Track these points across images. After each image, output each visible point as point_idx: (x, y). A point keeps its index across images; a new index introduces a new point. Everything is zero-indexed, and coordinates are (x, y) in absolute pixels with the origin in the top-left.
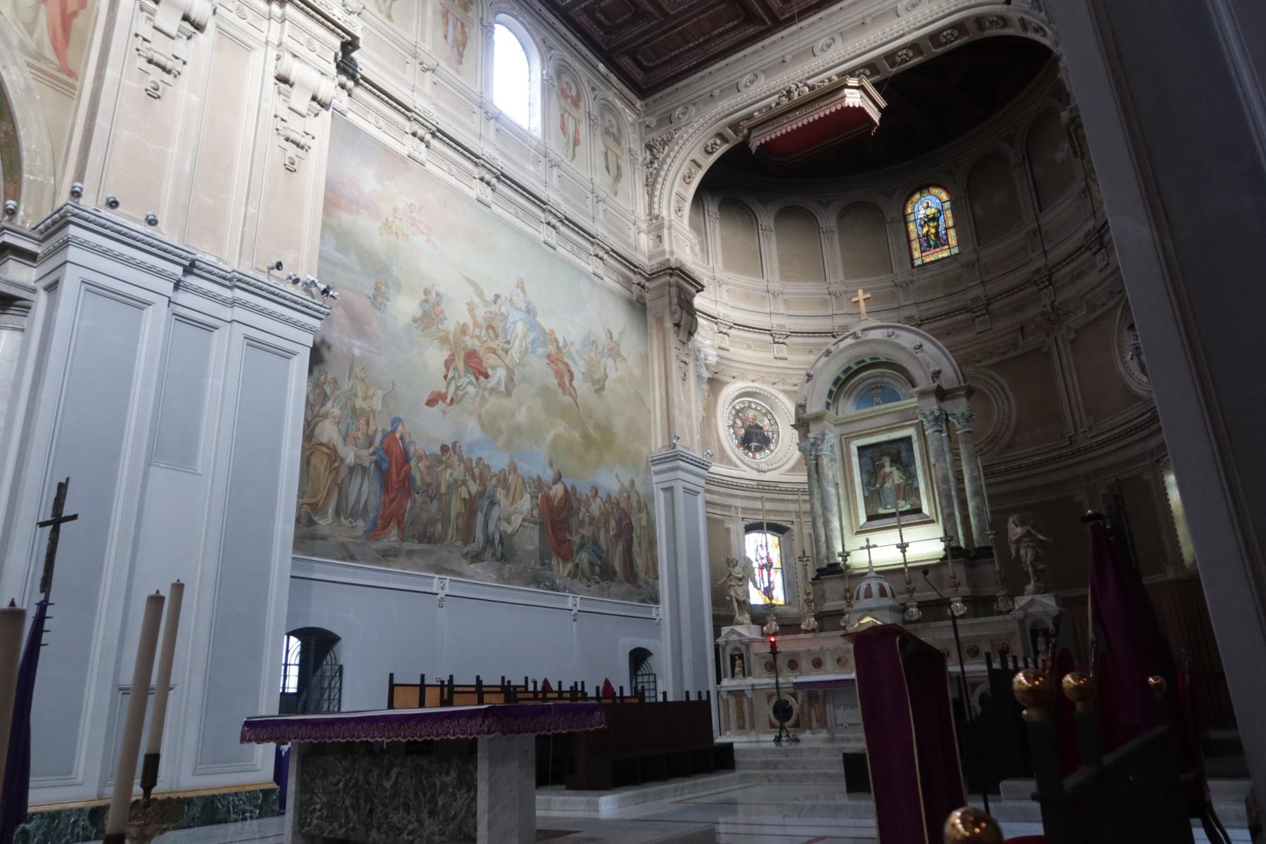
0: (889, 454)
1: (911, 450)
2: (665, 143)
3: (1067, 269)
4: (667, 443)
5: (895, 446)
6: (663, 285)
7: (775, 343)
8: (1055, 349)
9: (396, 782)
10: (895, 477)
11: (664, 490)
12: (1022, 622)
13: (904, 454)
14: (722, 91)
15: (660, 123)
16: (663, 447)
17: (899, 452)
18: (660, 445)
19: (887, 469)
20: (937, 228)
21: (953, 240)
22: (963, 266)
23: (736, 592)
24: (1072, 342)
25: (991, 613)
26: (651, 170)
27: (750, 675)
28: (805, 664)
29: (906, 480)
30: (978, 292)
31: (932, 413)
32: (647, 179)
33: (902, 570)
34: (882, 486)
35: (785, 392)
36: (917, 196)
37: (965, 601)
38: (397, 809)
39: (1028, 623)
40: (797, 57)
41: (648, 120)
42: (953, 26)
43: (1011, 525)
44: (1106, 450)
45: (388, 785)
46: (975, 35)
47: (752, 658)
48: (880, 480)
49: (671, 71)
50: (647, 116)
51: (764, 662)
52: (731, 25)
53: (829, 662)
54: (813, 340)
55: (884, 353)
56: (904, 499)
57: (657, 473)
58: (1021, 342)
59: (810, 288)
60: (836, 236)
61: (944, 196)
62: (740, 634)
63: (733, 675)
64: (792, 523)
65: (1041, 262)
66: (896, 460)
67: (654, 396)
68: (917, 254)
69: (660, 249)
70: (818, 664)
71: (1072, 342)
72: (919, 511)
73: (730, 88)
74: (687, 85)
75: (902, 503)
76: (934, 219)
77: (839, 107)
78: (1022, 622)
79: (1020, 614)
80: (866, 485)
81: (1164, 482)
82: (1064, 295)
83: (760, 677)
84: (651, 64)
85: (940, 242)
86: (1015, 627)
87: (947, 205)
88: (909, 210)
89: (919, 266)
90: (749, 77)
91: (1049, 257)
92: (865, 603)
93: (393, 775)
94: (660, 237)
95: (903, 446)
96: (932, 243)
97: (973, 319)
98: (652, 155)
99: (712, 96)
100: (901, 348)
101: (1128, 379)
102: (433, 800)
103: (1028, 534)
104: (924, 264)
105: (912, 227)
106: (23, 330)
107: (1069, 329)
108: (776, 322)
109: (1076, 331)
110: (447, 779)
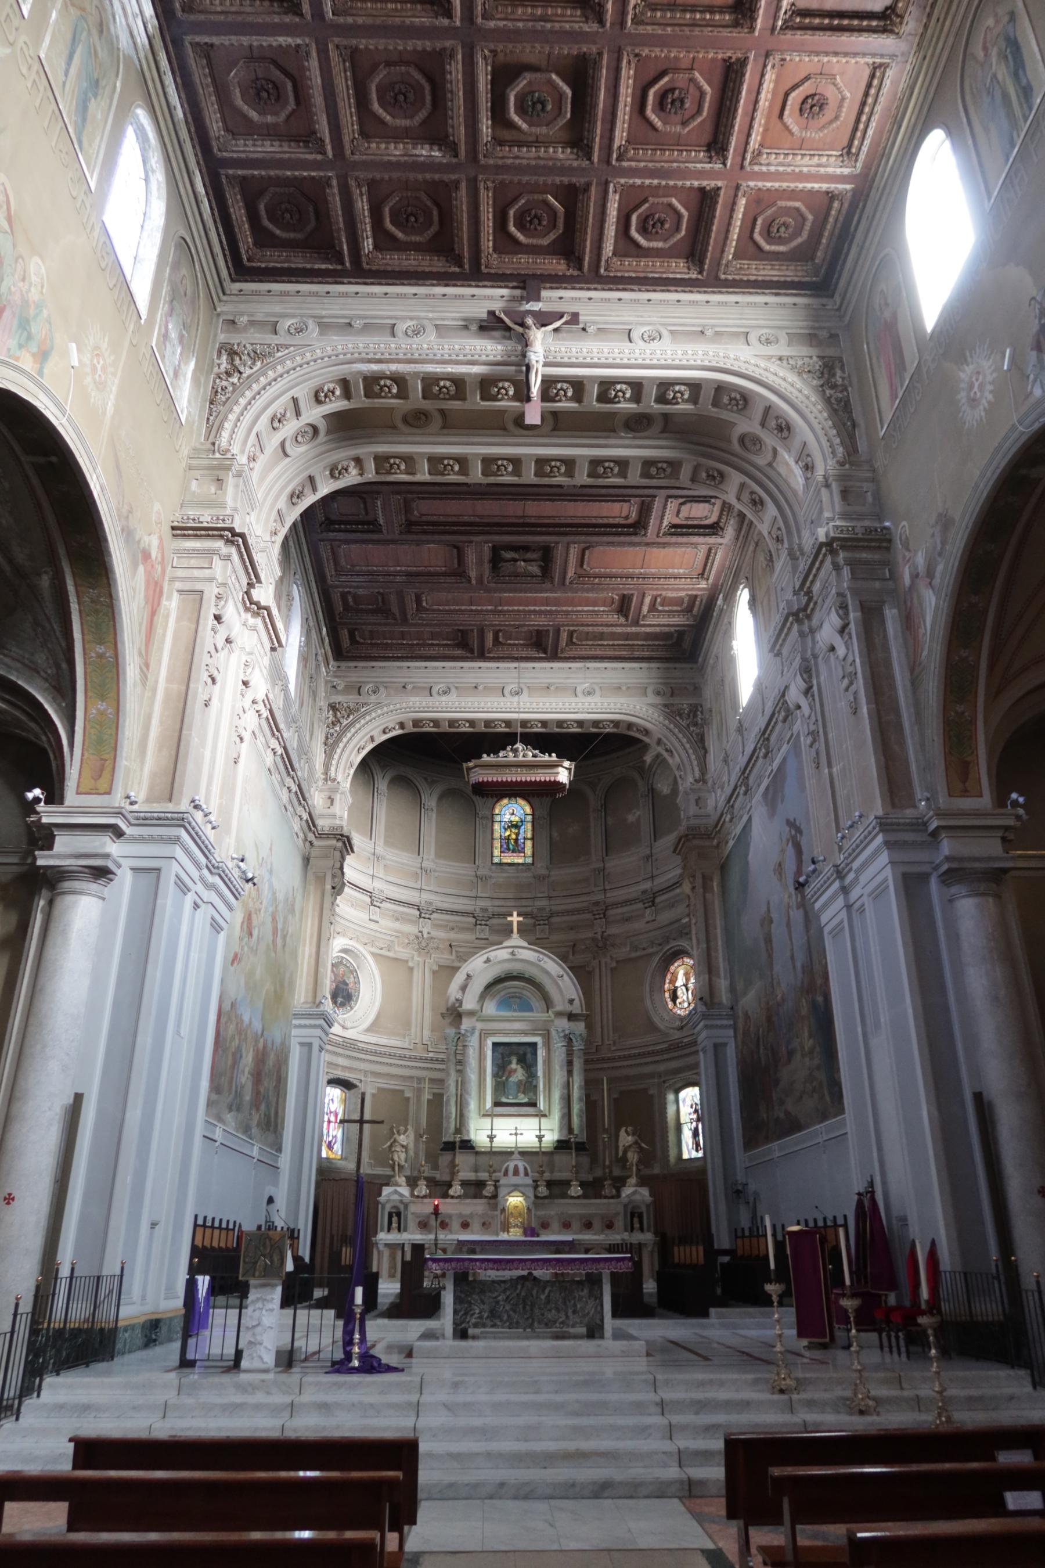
0: (517, 1054)
1: (535, 1054)
2: (350, 711)
3: (620, 910)
4: (310, 999)
5: (523, 1048)
6: (329, 847)
7: (372, 904)
8: (597, 971)
9: (549, 1296)
10: (519, 1074)
11: (302, 1044)
12: (625, 1206)
13: (529, 1056)
14: (414, 687)
15: (348, 690)
16: (305, 1003)
17: (525, 1054)
18: (302, 1000)
19: (514, 1066)
20: (517, 834)
21: (528, 850)
22: (534, 877)
23: (399, 1157)
24: (613, 970)
25: (600, 1197)
26: (332, 731)
27: (405, 1230)
28: (455, 1225)
29: (528, 1078)
30: (543, 903)
31: (563, 1031)
32: (327, 738)
33: (536, 1153)
34: (507, 1079)
35: (373, 954)
36: (505, 801)
37: (582, 1185)
38: (550, 1310)
39: (630, 1207)
40: (488, 690)
41: (336, 681)
42: (612, 721)
43: (622, 1133)
44: (625, 1063)
45: (543, 1297)
46: (622, 730)
47: (410, 1217)
48: (506, 1074)
49: (375, 652)
50: (336, 677)
51: (418, 1220)
52: (445, 642)
53: (476, 1225)
54: (401, 909)
55: (531, 971)
56: (524, 1093)
57: (296, 1026)
58: (571, 957)
59: (404, 858)
60: (434, 815)
61: (528, 810)
62: (401, 1195)
63: (389, 1230)
64: (361, 1081)
65: (599, 897)
66: (522, 1060)
67: (304, 951)
68: (496, 852)
69: (329, 811)
70: (465, 1225)
71: (613, 970)
72: (534, 1105)
73: (424, 688)
74: (384, 667)
75: (521, 1096)
76: (516, 826)
77: (552, 779)
78: (625, 1206)
79: (626, 1200)
80: (495, 1075)
81: (665, 1099)
82: (614, 930)
83: (413, 1233)
84: (362, 641)
85: (518, 849)
86: (621, 1209)
87: (529, 818)
88: (497, 811)
89: (497, 864)
90: (442, 687)
91: (608, 895)
92: (513, 1180)
93: (547, 1292)
94: (332, 801)
95: (529, 1050)
96: (511, 847)
97: (535, 925)
98: (335, 716)
99: (404, 687)
100: (547, 973)
101: (652, 1013)
102: (575, 1305)
103: (636, 1143)
104: (501, 864)
105: (496, 826)
106: (104, 899)
107: (612, 958)
108: (377, 885)
109: (617, 962)
110: (582, 1294)
